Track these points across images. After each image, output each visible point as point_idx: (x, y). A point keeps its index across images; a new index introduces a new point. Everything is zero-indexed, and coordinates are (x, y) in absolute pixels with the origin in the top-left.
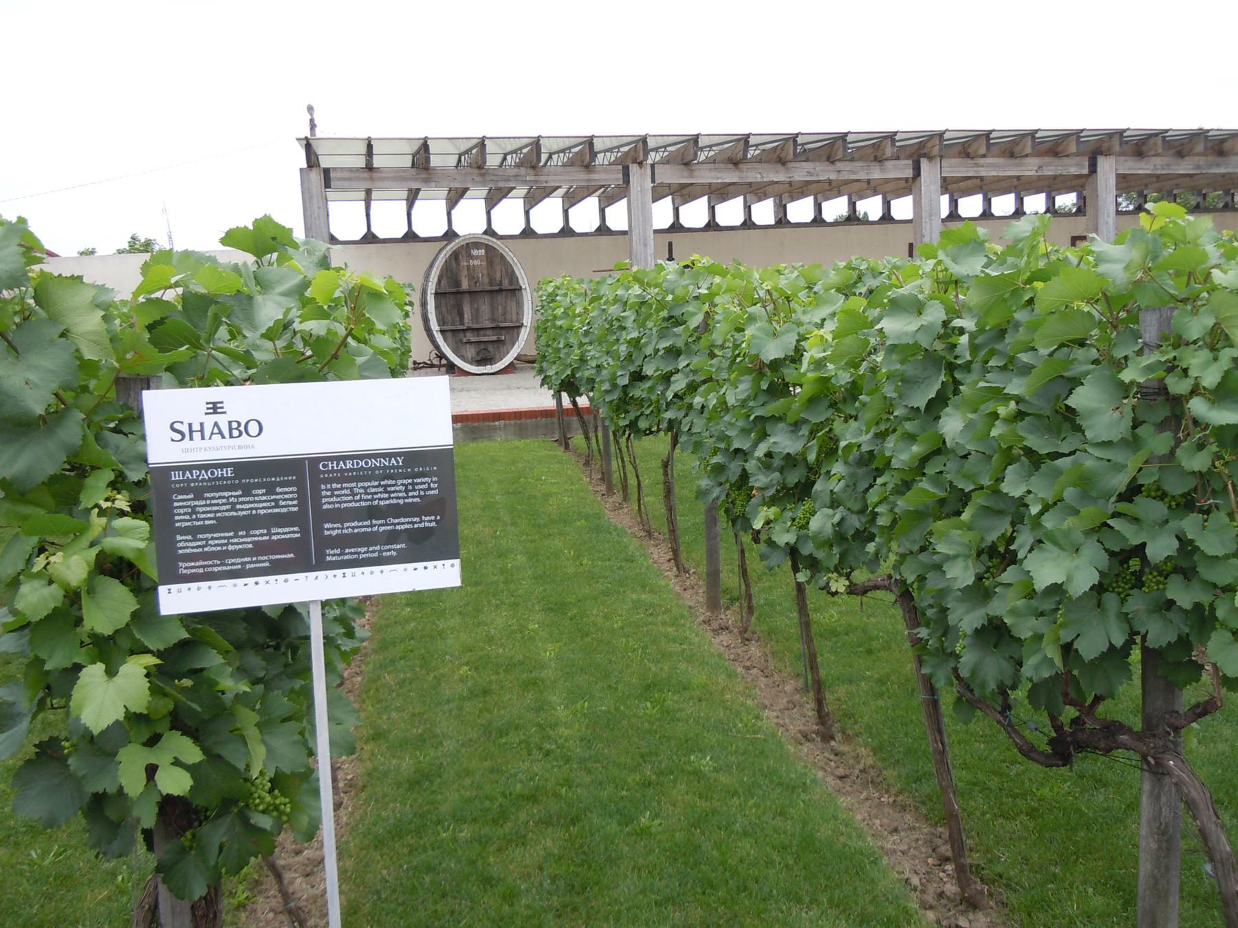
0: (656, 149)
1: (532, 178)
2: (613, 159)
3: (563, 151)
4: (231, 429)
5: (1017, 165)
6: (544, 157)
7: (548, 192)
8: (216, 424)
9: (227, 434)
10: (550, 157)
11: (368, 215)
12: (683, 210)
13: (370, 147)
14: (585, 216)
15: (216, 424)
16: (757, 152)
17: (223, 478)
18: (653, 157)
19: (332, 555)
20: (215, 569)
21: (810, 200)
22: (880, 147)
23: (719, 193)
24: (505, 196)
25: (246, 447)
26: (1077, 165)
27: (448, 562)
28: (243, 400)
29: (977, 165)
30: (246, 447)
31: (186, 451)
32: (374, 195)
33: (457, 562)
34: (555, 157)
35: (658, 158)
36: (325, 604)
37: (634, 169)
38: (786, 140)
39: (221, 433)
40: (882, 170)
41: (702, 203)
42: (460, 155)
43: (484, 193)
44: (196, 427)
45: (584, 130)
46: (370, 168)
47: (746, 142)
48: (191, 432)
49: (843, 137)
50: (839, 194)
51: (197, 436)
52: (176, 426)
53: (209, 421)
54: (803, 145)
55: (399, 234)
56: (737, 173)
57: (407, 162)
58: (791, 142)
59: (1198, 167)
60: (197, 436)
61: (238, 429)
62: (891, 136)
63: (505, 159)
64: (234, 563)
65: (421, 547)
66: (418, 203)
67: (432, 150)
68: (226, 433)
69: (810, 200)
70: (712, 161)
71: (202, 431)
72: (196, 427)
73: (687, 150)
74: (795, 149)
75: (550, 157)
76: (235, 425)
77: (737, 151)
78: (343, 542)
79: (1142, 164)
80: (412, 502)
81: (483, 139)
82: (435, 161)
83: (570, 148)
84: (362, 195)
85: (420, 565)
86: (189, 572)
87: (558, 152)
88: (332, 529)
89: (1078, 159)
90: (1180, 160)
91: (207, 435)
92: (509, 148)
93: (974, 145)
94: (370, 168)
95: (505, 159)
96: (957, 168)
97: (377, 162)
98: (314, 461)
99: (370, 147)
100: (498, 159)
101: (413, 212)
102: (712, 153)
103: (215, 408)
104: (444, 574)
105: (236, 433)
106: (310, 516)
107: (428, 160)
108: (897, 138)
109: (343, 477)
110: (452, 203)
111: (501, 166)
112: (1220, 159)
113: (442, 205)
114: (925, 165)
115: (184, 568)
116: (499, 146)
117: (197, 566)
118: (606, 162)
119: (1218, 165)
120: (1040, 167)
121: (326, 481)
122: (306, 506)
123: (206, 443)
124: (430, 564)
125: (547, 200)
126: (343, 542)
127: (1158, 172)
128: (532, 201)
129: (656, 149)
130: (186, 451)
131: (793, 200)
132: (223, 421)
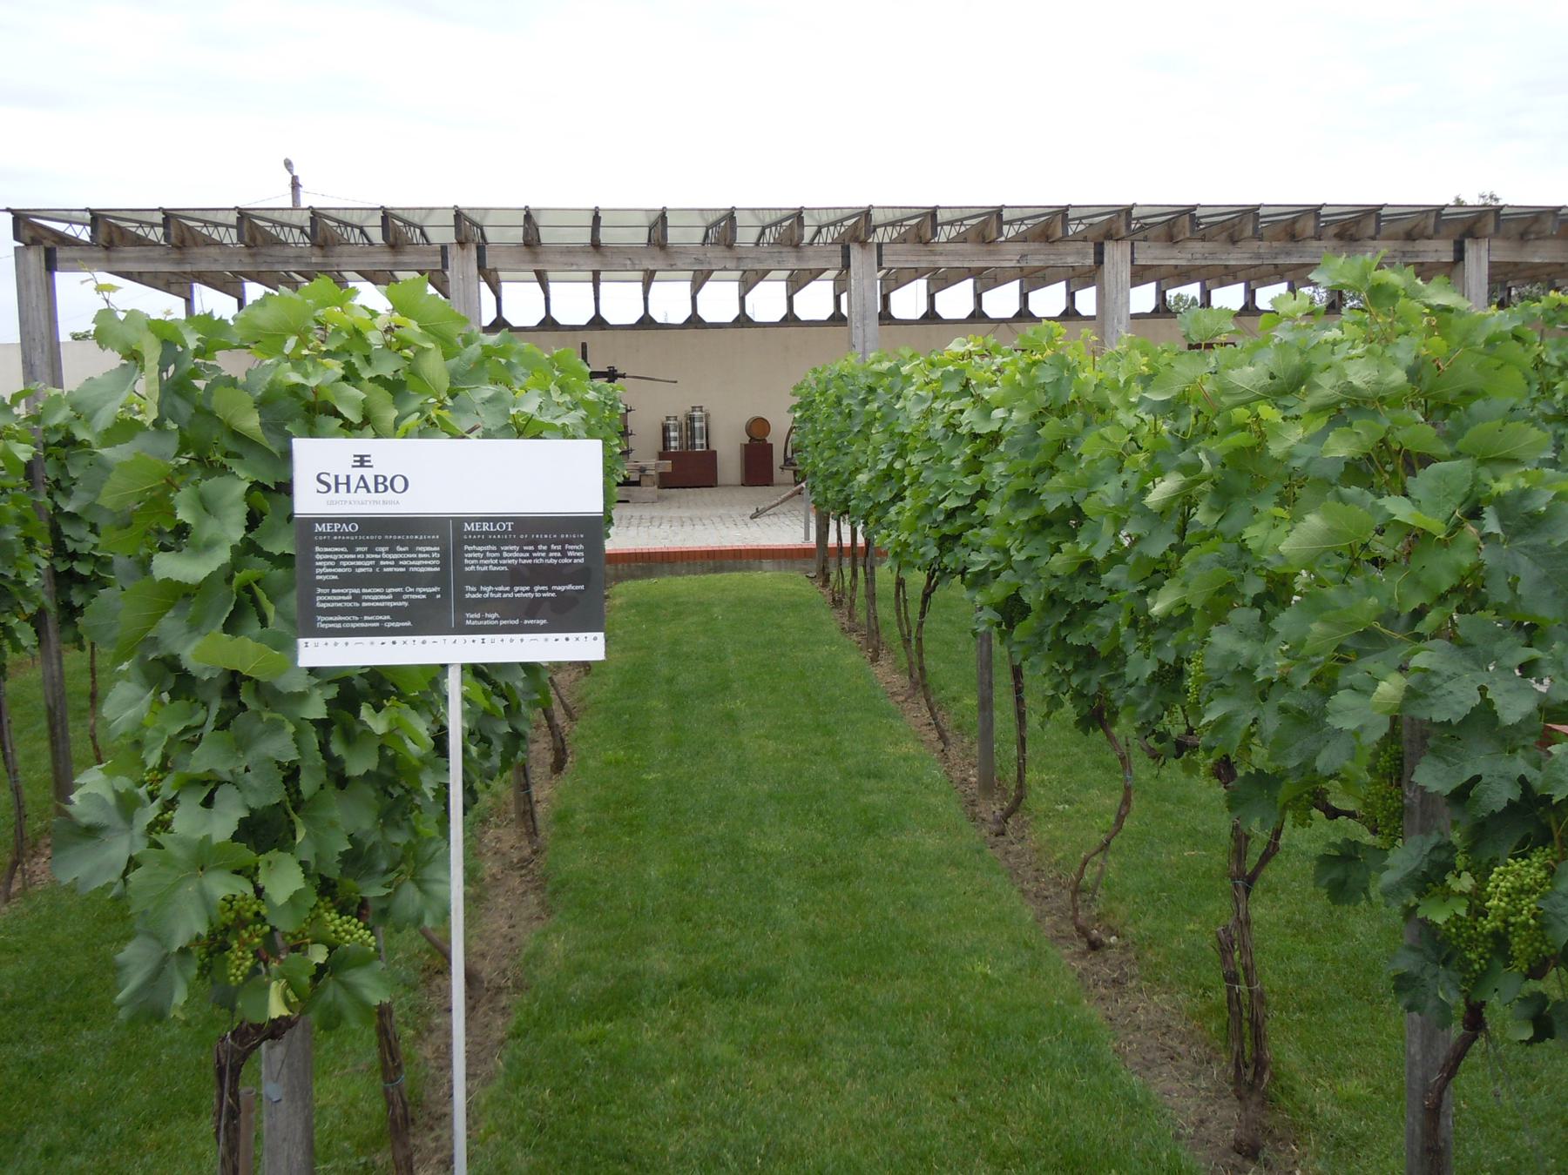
0: (1010, 223)
1: (320, 260)
2: (895, 235)
3: (834, 224)
4: (376, 484)
5: (990, 253)
6: (808, 233)
7: (815, 274)
8: (362, 478)
9: (372, 488)
10: (819, 232)
11: (597, 299)
12: (987, 297)
13: (596, 219)
14: (816, 301)
15: (362, 478)
16: (1081, 227)
17: (344, 534)
18: (880, 235)
19: (472, 618)
20: (353, 625)
21: (1153, 286)
22: (1241, 224)
23: (1033, 279)
24: (762, 279)
25: (391, 502)
26: (1078, 253)
27: (591, 635)
28: (388, 454)
29: (933, 253)
30: (391, 502)
31: (331, 503)
32: (603, 275)
33: (600, 635)
34: (824, 230)
35: (1012, 233)
36: (463, 667)
37: (855, 251)
38: (1055, 214)
39: (366, 486)
40: (799, 259)
41: (1012, 289)
42: (764, 229)
43: (738, 274)
44: (342, 479)
45: (857, 199)
46: (596, 244)
47: (1000, 216)
48: (337, 484)
49: (1127, 211)
50: (1236, 281)
51: (343, 488)
52: (323, 477)
53: (356, 474)
54: (1138, 219)
55: (633, 319)
56: (599, 258)
57: (642, 237)
58: (1123, 216)
59: (1258, 256)
60: (343, 488)
61: (384, 484)
62: (1315, 211)
63: (763, 233)
64: (370, 621)
65: (564, 617)
66: (655, 286)
67: (669, 222)
68: (372, 486)
69: (1153, 286)
70: (1022, 238)
71: (348, 484)
72: (342, 479)
73: (988, 225)
74: (1128, 225)
75: (819, 232)
76: (381, 480)
77: (1051, 226)
78: (482, 605)
79: (1175, 252)
80: (554, 568)
81: (802, 209)
82: (673, 236)
83: (842, 221)
84: (589, 275)
85: (562, 636)
86: (327, 626)
87: (885, 225)
88: (471, 593)
89: (1079, 245)
90: (1230, 247)
91: (353, 488)
92: (768, 220)
93: (1180, 224)
94: (596, 244)
95: (763, 233)
96: (1150, 254)
97: (605, 237)
98: (459, 521)
99: (596, 219)
100: (755, 232)
101: (650, 296)
102: (1023, 228)
103: (362, 461)
104: (588, 647)
105: (381, 488)
106: (450, 575)
107: (665, 236)
108: (1323, 212)
109: (483, 539)
110: (746, 286)
111: (757, 244)
112: (1290, 245)
113: (685, 288)
114: (1109, 247)
115: (322, 622)
116: (757, 217)
117: (336, 621)
118: (887, 240)
119: (1288, 254)
120: (1023, 256)
121: (470, 543)
122: (444, 568)
123: (352, 496)
124: (572, 636)
125: (813, 283)
126: (482, 605)
127: (1197, 263)
128: (796, 283)
129: (1010, 223)
130: (331, 503)
131: (1222, 285)
132: (370, 475)
